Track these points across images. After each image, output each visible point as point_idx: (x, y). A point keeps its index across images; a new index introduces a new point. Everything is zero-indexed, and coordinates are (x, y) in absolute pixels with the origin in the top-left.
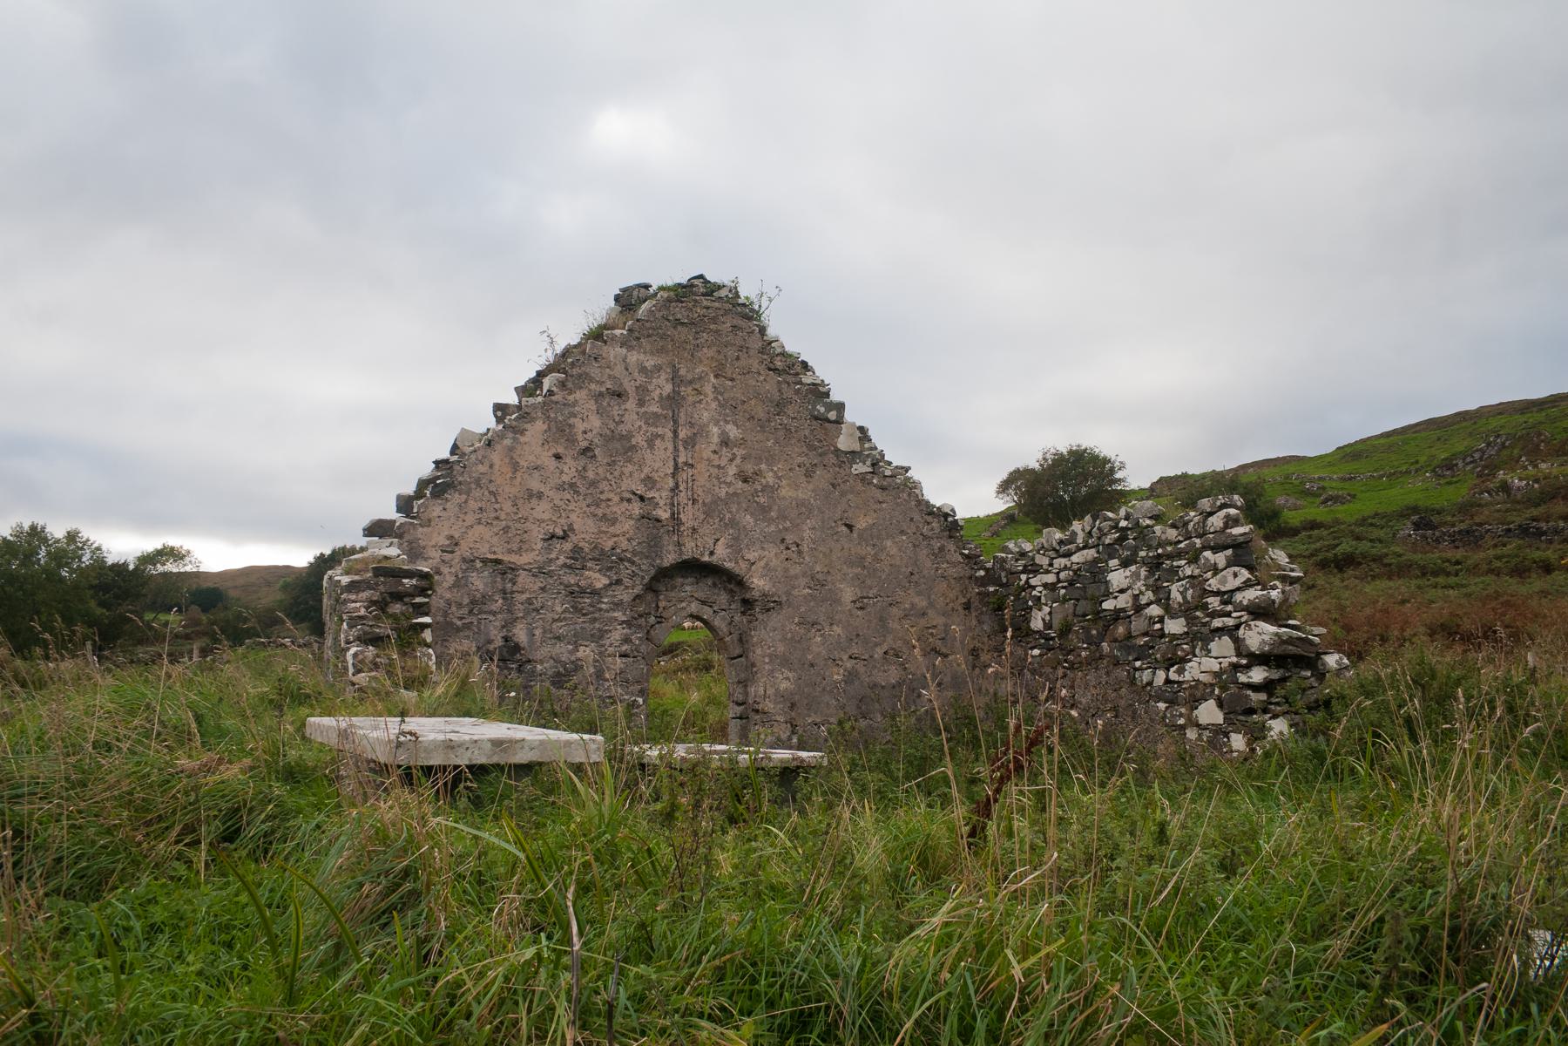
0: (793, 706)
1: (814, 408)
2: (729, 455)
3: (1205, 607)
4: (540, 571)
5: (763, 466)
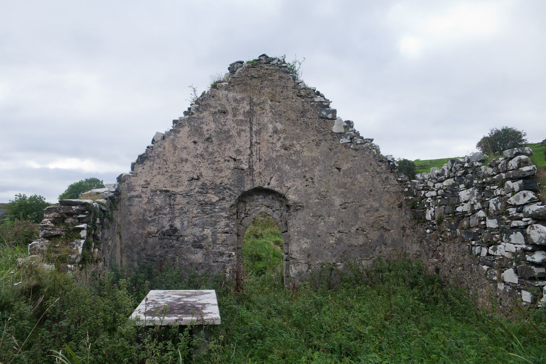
0: (309, 256)
1: (321, 113)
2: (277, 137)
3: (507, 213)
4: (187, 195)
5: (295, 142)
